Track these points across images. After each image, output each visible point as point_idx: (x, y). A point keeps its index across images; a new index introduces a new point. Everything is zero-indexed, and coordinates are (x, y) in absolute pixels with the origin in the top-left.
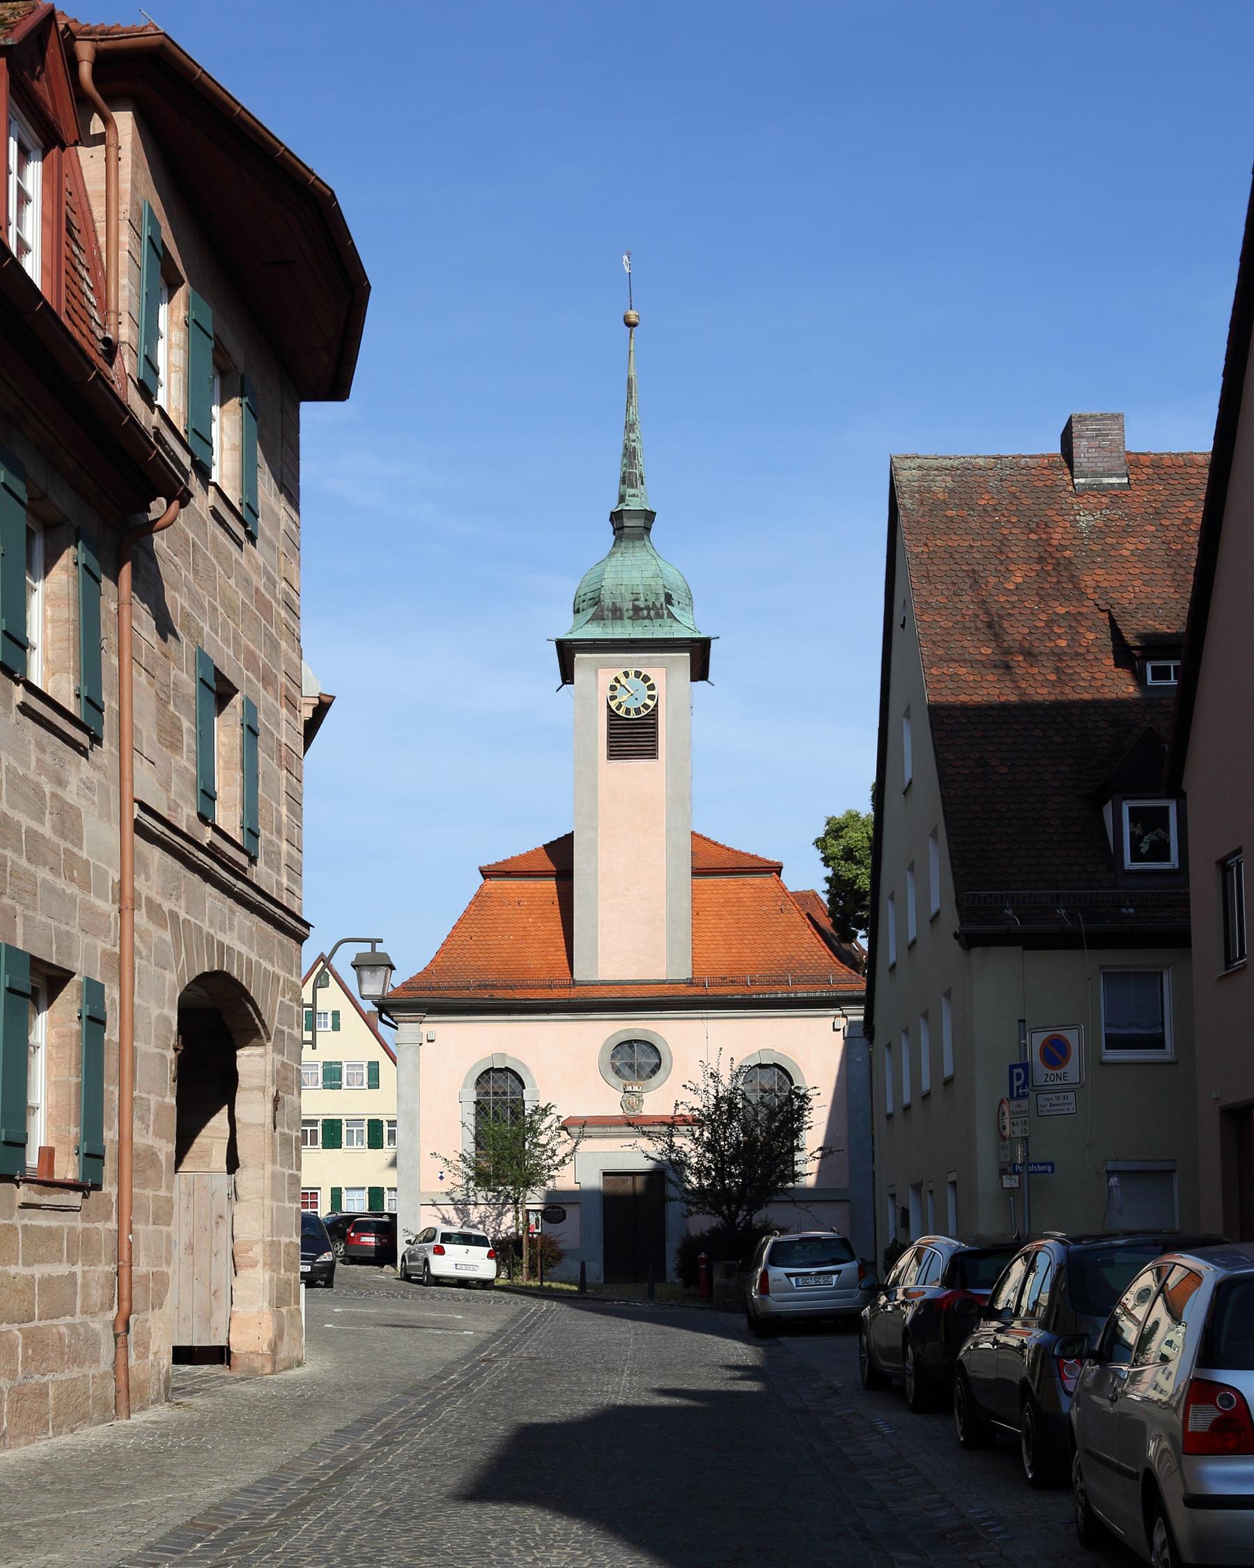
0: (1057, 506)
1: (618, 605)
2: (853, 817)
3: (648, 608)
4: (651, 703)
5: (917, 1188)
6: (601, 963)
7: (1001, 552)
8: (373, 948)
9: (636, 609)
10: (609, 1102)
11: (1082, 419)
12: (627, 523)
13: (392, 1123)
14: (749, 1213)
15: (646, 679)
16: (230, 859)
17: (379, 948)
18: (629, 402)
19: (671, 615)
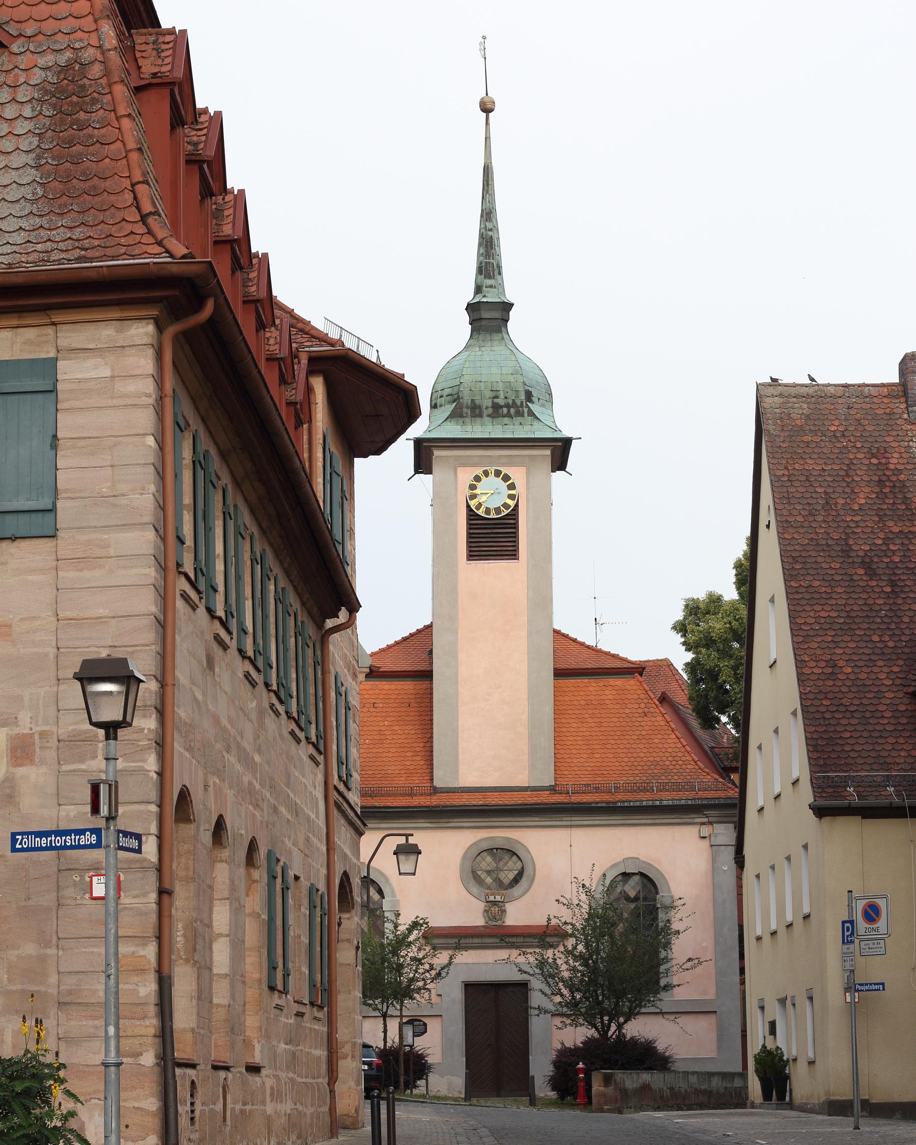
0: (894, 433)
1: (477, 402)
2: (715, 601)
3: (508, 406)
5: (782, 1001)
6: (463, 769)
7: (848, 475)
8: (407, 840)
9: (496, 407)
10: (468, 912)
15: (506, 478)
18: (487, 172)
19: (531, 414)
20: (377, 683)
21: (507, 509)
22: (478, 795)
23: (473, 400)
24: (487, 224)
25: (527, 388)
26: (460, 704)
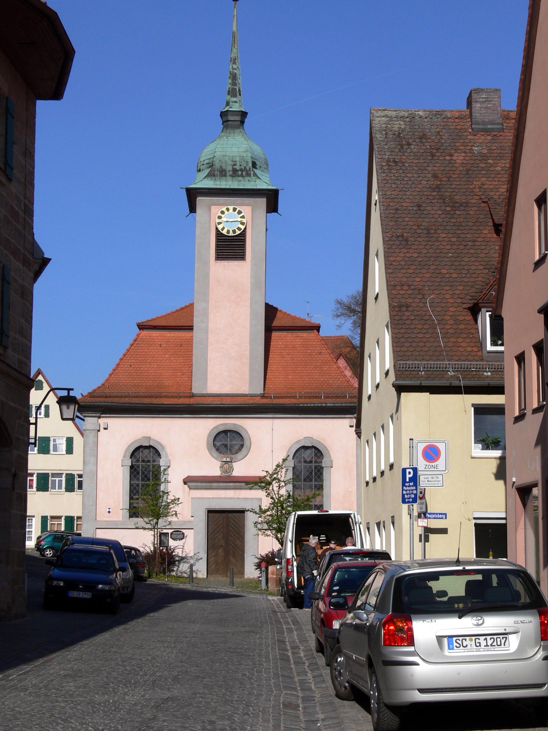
1: (224, 168)
3: (241, 170)
5: (378, 524)
6: (210, 383)
8: (69, 393)
9: (235, 171)
10: (212, 467)
11: (478, 91)
12: (230, 118)
13: (80, 476)
17: (72, 394)
19: (255, 175)
20: (163, 333)
21: (240, 230)
22: (219, 399)
23: (221, 167)
24: (234, 65)
25: (253, 160)
26: (209, 344)
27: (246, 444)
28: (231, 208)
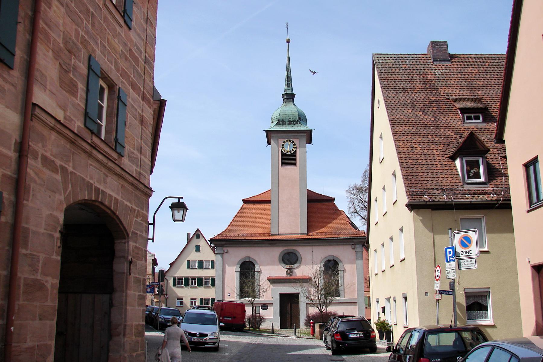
4: (295, 149)
5: (388, 300)
8: (179, 200)
14: (327, 307)
15: (293, 142)
16: (105, 152)
17: (181, 201)
18: (288, 59)
27: (299, 259)
28: (289, 141)
